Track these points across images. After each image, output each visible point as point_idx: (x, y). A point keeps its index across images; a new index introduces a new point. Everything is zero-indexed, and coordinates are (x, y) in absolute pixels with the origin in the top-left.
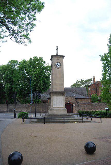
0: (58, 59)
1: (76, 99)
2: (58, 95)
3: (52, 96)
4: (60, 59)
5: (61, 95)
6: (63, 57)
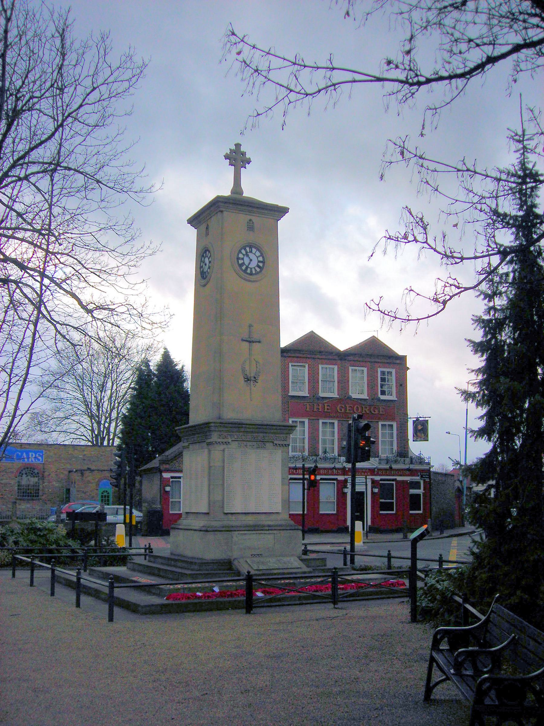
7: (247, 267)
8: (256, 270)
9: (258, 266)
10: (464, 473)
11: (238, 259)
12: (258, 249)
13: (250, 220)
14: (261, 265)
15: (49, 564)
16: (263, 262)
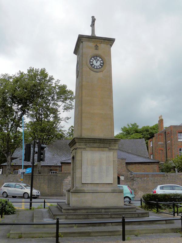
0: (96, 47)
1: (128, 164)
2: (97, 149)
3: (79, 151)
4: (102, 46)
5: (107, 149)
6: (110, 41)
8: (99, 67)
9: (100, 65)
11: (90, 62)
13: (96, 45)
14: (102, 64)
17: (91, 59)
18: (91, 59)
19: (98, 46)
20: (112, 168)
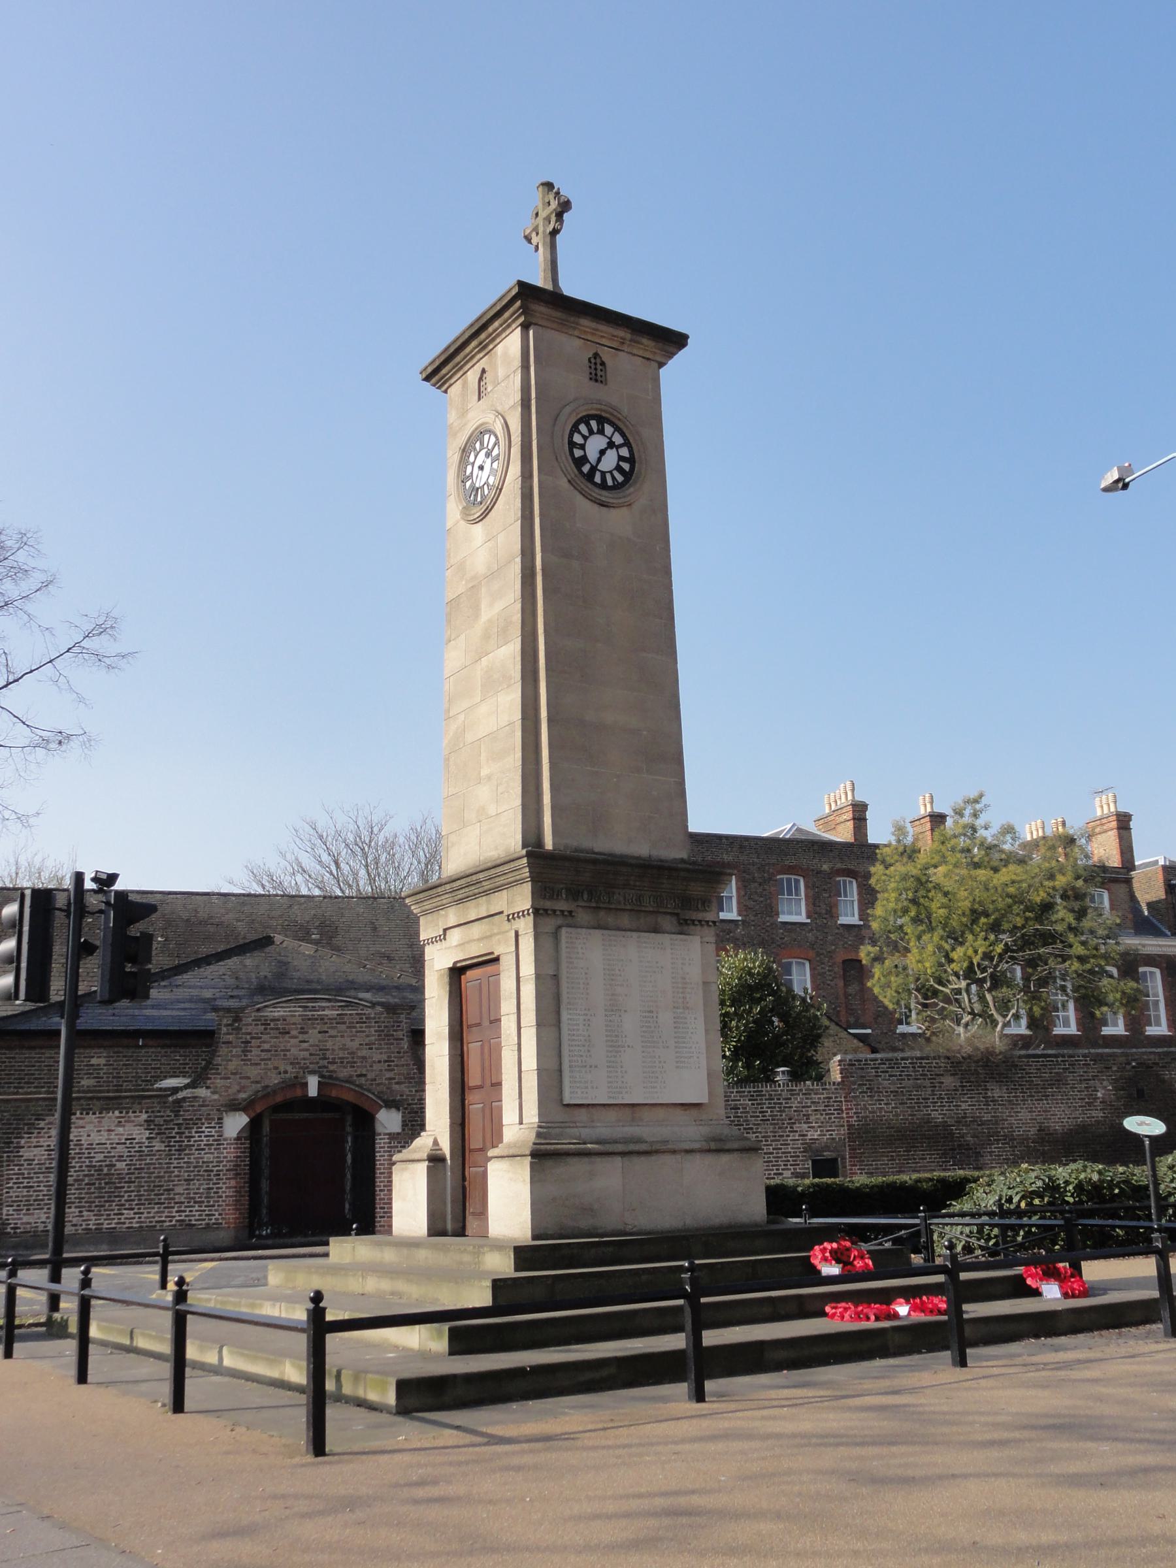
4: (623, 364)
7: (594, 469)
8: (614, 478)
10: (1070, 893)
11: (572, 445)
12: (617, 429)
13: (596, 355)
14: (626, 466)
15: (800, 1217)
16: (631, 460)
17: (575, 429)
18: (575, 429)
19: (603, 364)
20: (701, 1020)
